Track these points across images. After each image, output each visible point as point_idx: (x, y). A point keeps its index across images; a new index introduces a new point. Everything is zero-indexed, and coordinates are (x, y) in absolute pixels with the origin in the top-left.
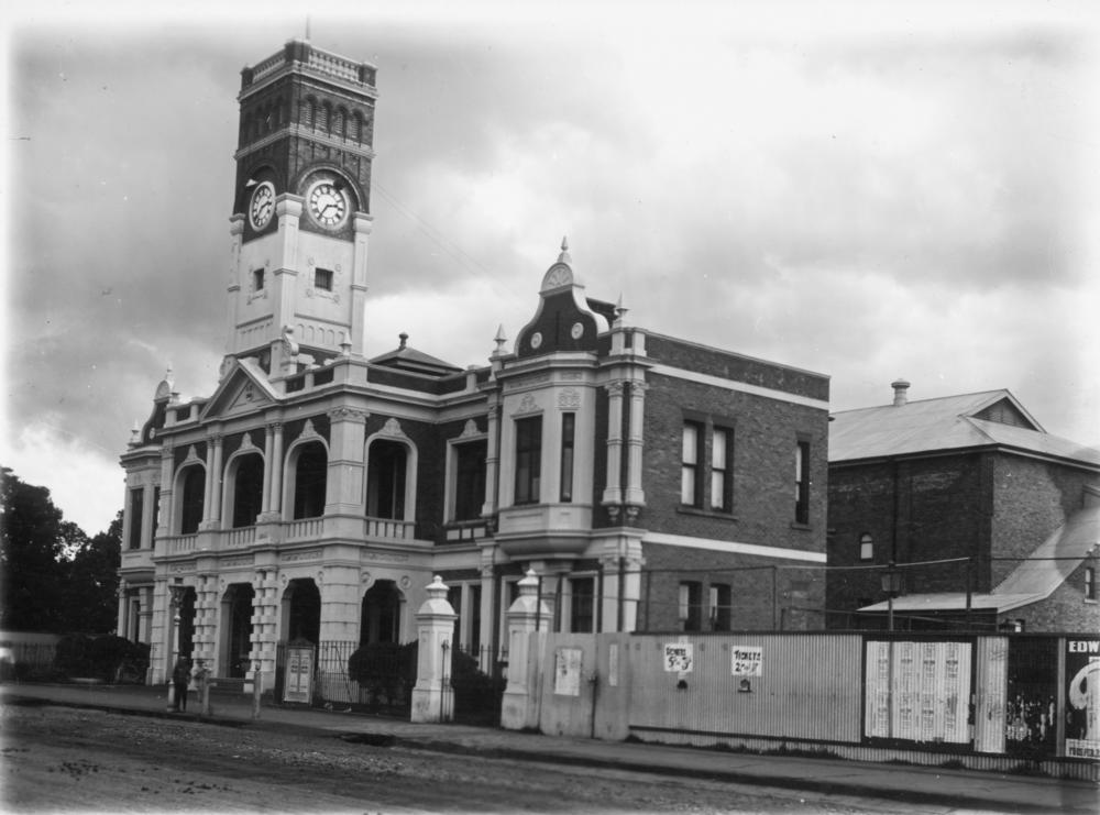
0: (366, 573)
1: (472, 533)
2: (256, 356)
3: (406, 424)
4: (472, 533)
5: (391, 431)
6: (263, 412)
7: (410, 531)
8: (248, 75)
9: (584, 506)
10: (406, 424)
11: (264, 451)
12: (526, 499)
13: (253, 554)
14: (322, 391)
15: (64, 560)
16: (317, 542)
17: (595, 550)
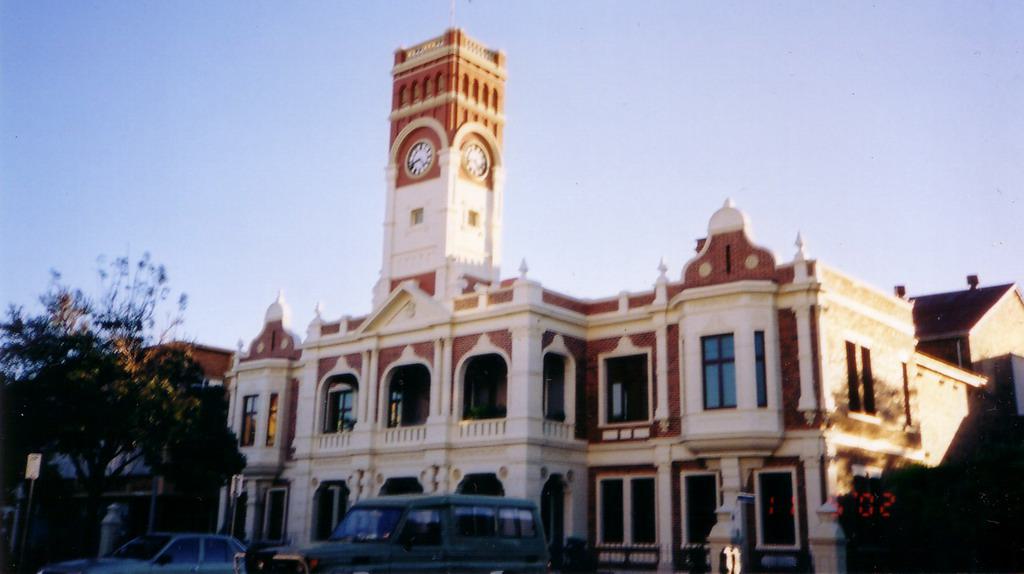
1: (632, 433)
2: (485, 263)
3: (569, 341)
4: (632, 433)
5: (558, 346)
7: (571, 432)
8: (401, 56)
10: (569, 341)
11: (360, 373)
12: (717, 404)
13: (424, 450)
15: (146, 464)
17: (789, 450)
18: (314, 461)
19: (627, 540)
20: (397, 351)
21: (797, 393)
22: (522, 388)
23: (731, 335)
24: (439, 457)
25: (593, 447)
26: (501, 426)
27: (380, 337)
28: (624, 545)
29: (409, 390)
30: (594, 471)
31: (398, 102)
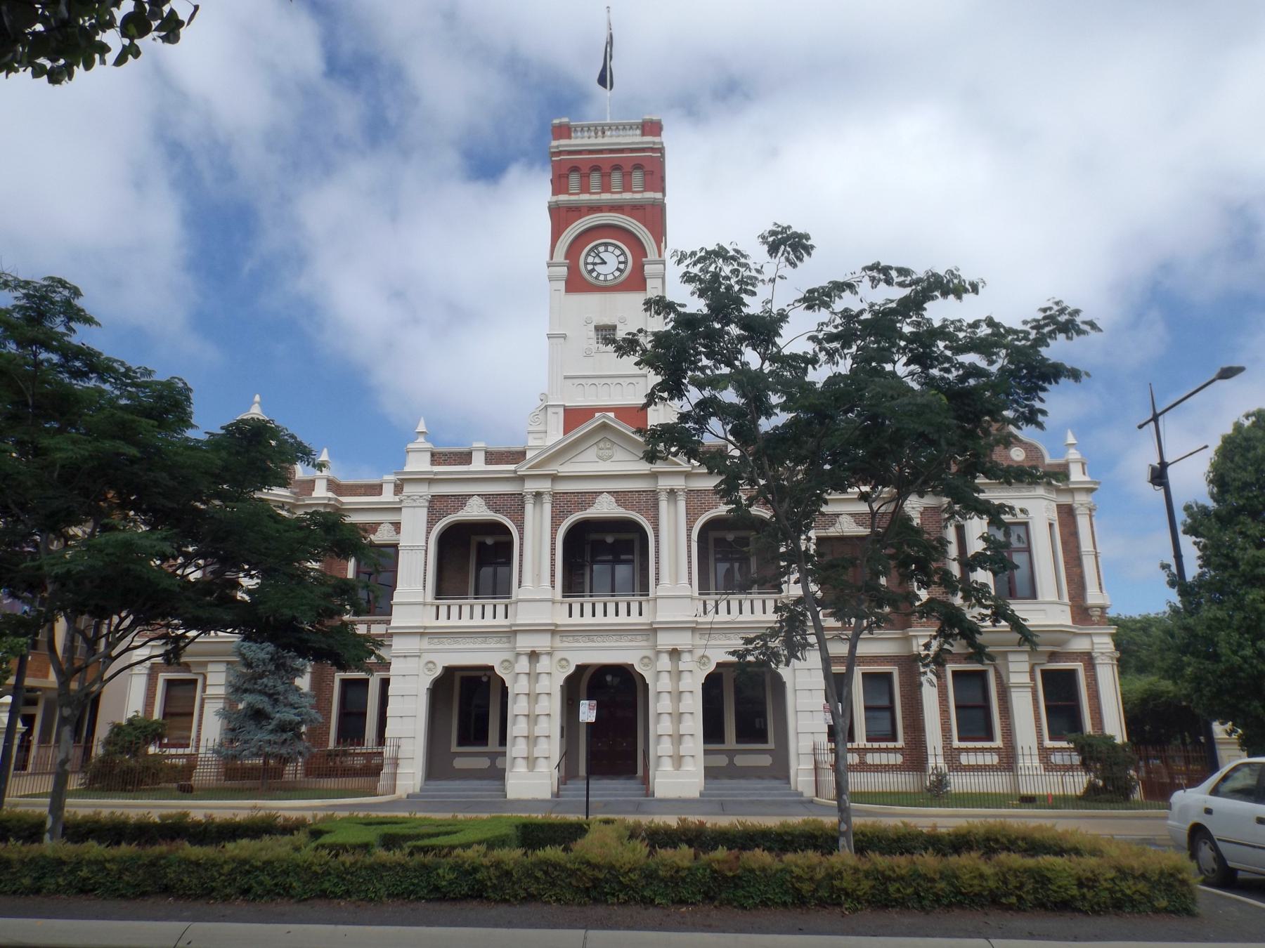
20: (589, 498)
27: (555, 478)
28: (855, 745)
29: (475, 557)
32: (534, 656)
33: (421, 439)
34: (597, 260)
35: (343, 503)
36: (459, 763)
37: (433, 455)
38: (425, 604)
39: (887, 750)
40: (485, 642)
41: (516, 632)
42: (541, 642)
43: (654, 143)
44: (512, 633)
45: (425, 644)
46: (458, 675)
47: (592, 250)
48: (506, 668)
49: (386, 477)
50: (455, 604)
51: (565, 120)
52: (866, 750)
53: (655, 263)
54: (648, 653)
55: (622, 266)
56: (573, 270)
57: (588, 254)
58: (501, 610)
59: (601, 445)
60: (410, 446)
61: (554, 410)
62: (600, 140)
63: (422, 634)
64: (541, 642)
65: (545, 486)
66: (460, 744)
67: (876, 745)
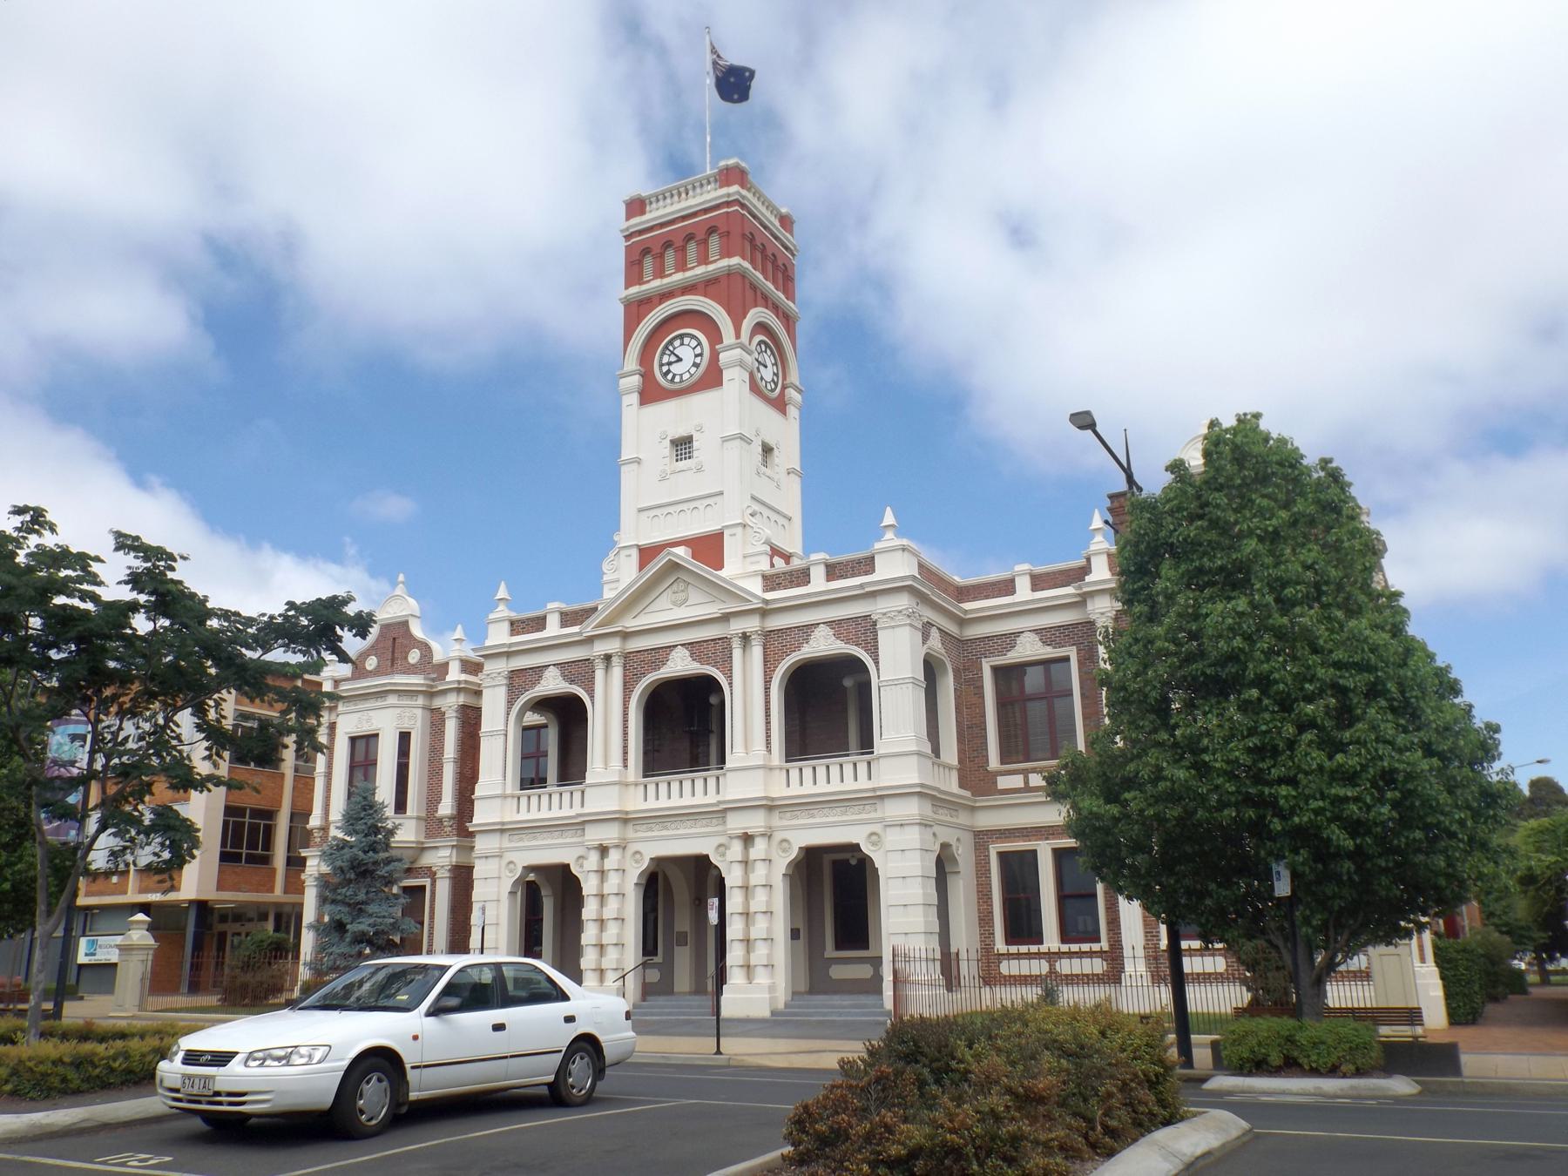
0: (637, 852)
6: (726, 618)
9: (418, 818)
14: (861, 586)
16: (874, 790)
18: (630, 826)
19: (1051, 940)
20: (660, 655)
21: (307, 814)
22: (897, 710)
23: (377, 735)
24: (609, 834)
25: (982, 801)
26: (577, 796)
27: (625, 635)
28: (1043, 948)
29: (683, 723)
30: (982, 838)
31: (634, 273)
32: (747, 839)
33: (889, 535)
34: (673, 359)
35: (966, 612)
36: (837, 972)
37: (512, 623)
38: (504, 797)
39: (1029, 956)
40: (844, 813)
41: (881, 797)
42: (754, 822)
43: (729, 195)
44: (721, 813)
45: (506, 841)
46: (827, 860)
47: (666, 347)
48: (874, 844)
49: (1018, 568)
50: (807, 766)
51: (731, 162)
52: (1060, 955)
53: (730, 348)
54: (722, 840)
55: (698, 360)
56: (647, 375)
57: (663, 353)
58: (862, 768)
59: (675, 587)
60: (491, 616)
61: (627, 552)
62: (644, 218)
63: (502, 831)
64: (754, 822)
65: (612, 646)
66: (838, 947)
67: (1075, 947)
